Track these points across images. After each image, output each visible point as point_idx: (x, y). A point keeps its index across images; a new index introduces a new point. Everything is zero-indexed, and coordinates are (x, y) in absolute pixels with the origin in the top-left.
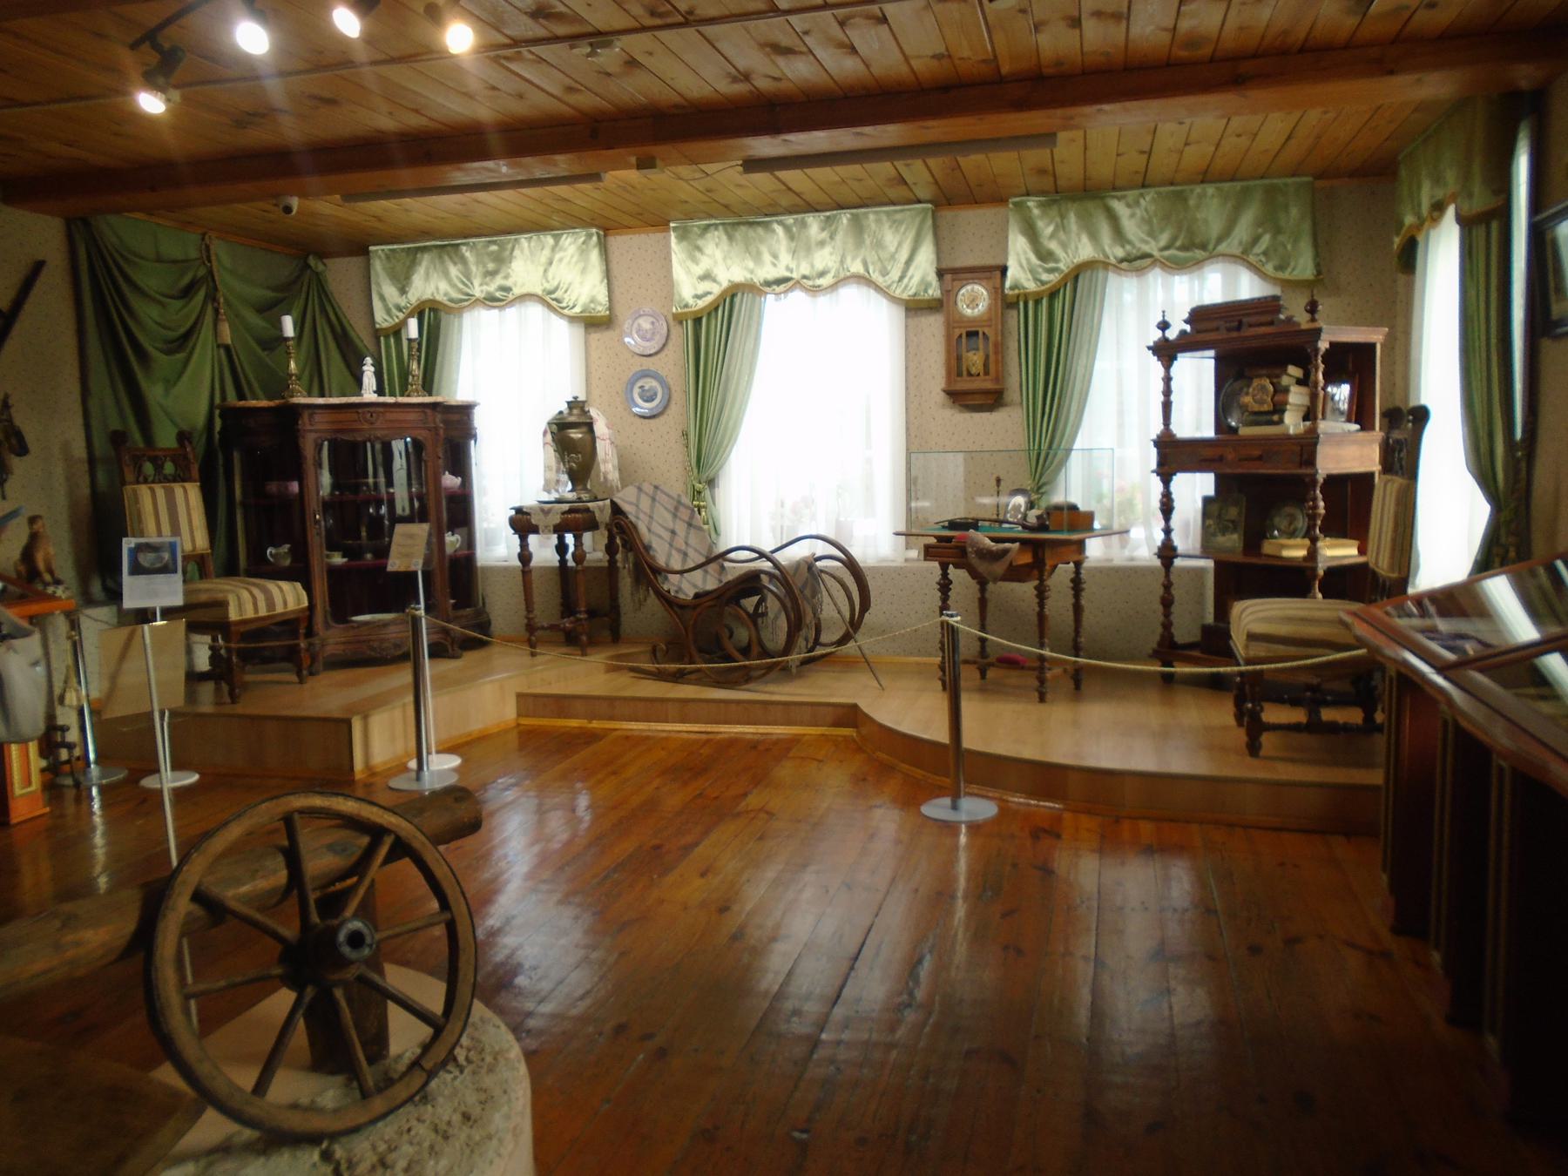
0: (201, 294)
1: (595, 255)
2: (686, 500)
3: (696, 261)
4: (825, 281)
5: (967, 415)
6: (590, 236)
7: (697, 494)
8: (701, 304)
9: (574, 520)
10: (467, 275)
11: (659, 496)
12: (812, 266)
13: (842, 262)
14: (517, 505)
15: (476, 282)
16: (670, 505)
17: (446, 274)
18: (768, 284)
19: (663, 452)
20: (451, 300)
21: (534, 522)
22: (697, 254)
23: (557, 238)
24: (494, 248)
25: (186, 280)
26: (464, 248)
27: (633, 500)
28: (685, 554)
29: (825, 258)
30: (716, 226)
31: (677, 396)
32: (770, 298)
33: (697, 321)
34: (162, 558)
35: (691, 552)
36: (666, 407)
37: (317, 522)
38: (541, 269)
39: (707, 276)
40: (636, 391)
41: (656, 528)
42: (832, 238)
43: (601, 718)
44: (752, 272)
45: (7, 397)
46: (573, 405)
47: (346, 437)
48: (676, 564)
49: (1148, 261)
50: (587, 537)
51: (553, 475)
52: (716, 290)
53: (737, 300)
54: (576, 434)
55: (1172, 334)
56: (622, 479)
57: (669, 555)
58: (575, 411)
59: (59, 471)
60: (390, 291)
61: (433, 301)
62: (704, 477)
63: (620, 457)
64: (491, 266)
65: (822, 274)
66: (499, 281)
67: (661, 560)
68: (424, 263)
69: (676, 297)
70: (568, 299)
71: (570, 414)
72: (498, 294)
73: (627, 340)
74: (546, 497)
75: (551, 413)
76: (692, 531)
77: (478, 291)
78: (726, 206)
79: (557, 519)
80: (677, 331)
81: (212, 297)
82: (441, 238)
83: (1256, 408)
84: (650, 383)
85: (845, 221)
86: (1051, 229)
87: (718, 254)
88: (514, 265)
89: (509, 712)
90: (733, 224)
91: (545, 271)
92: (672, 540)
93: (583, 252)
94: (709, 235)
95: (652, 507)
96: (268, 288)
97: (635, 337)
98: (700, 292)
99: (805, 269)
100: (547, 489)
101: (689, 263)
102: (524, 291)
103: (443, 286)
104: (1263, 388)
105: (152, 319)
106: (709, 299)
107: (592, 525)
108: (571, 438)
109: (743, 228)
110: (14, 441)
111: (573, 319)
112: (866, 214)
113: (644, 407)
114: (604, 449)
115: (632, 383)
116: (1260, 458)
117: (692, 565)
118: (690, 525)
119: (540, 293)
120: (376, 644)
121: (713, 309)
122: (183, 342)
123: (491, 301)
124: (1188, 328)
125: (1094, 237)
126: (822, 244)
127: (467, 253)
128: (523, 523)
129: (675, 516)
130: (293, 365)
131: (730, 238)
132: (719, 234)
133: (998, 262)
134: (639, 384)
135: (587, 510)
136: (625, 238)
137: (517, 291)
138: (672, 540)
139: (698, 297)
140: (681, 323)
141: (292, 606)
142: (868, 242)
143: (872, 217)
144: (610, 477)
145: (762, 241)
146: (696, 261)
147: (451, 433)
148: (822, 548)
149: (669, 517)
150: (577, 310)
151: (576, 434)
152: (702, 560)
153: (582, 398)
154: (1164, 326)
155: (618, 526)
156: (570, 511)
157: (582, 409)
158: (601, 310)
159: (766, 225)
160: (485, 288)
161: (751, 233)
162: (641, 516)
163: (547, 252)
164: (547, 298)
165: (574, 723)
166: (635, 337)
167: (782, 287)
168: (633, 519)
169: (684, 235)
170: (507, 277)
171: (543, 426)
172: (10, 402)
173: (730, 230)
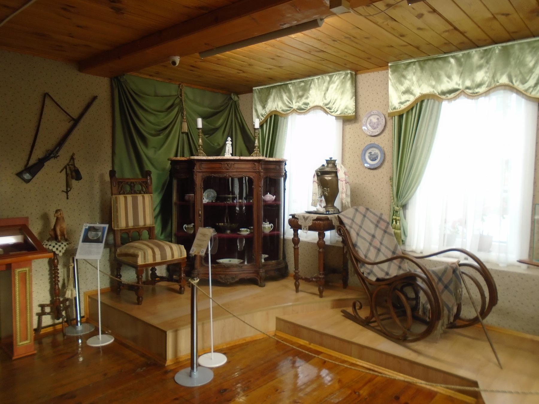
0: (176, 110)
1: (348, 84)
2: (386, 217)
3: (401, 83)
6: (347, 74)
7: (395, 212)
8: (403, 107)
10: (290, 98)
11: (369, 214)
12: (473, 81)
13: (493, 77)
14: (293, 213)
15: (294, 102)
16: (375, 219)
17: (281, 98)
18: (443, 93)
19: (379, 188)
20: (283, 111)
21: (299, 223)
22: (403, 79)
23: (331, 77)
24: (303, 84)
25: (169, 104)
26: (290, 85)
28: (379, 250)
29: (480, 76)
30: (414, 62)
31: (388, 158)
32: (445, 104)
33: (401, 117)
34: (97, 235)
35: (383, 249)
37: (199, 215)
38: (323, 93)
39: (408, 91)
41: (362, 233)
43: (315, 343)
44: (434, 87)
45: (73, 154)
47: (216, 175)
48: (372, 256)
50: (328, 234)
51: (318, 197)
52: (412, 99)
53: (424, 104)
54: (328, 178)
56: (352, 201)
57: (368, 250)
58: (330, 165)
59: (97, 187)
60: (259, 108)
61: (276, 111)
62: (400, 204)
63: (352, 191)
64: (300, 93)
65: (479, 85)
66: (304, 100)
67: (362, 255)
68: (273, 94)
69: (390, 104)
70: (335, 107)
71: (327, 166)
72: (303, 107)
73: (364, 128)
75: (318, 166)
76: (386, 235)
77: (295, 106)
78: (418, 48)
79: (310, 223)
81: (181, 110)
82: (280, 81)
84: (375, 151)
85: (497, 51)
87: (414, 78)
88: (311, 92)
89: (271, 327)
90: (424, 61)
91: (325, 94)
92: (372, 241)
93: (343, 83)
94: (410, 68)
95: (363, 221)
96: (210, 108)
97: (368, 125)
98: (403, 100)
99: (468, 83)
100: (314, 204)
101: (397, 85)
102: (315, 104)
103: (280, 104)
105: (149, 122)
106: (408, 104)
107: (331, 227)
109: (430, 62)
110: (74, 174)
111: (337, 117)
112: (512, 46)
113: (370, 162)
114: (342, 186)
117: (383, 258)
118: (385, 232)
119: (321, 104)
120: (223, 276)
121: (410, 109)
122: (165, 130)
123: (301, 111)
126: (480, 67)
127: (291, 87)
128: (295, 223)
129: (377, 226)
130: (200, 141)
131: (422, 68)
132: (417, 67)
134: (369, 151)
135: (327, 219)
136: (367, 74)
137: (311, 105)
138: (372, 241)
139: (402, 103)
141: (177, 256)
142: (513, 63)
143: (517, 47)
145: (441, 68)
146: (401, 83)
147: (273, 176)
148: (463, 259)
149: (372, 226)
150: (338, 113)
151: (328, 178)
152: (390, 255)
156: (318, 219)
158: (351, 112)
159: (445, 59)
160: (298, 104)
161: (435, 64)
162: (354, 226)
163: (326, 84)
164: (325, 108)
165: (302, 342)
166: (368, 125)
167: (452, 95)
168: (348, 227)
169: (395, 69)
170: (307, 98)
171: (314, 172)
172: (75, 157)
173: (422, 64)
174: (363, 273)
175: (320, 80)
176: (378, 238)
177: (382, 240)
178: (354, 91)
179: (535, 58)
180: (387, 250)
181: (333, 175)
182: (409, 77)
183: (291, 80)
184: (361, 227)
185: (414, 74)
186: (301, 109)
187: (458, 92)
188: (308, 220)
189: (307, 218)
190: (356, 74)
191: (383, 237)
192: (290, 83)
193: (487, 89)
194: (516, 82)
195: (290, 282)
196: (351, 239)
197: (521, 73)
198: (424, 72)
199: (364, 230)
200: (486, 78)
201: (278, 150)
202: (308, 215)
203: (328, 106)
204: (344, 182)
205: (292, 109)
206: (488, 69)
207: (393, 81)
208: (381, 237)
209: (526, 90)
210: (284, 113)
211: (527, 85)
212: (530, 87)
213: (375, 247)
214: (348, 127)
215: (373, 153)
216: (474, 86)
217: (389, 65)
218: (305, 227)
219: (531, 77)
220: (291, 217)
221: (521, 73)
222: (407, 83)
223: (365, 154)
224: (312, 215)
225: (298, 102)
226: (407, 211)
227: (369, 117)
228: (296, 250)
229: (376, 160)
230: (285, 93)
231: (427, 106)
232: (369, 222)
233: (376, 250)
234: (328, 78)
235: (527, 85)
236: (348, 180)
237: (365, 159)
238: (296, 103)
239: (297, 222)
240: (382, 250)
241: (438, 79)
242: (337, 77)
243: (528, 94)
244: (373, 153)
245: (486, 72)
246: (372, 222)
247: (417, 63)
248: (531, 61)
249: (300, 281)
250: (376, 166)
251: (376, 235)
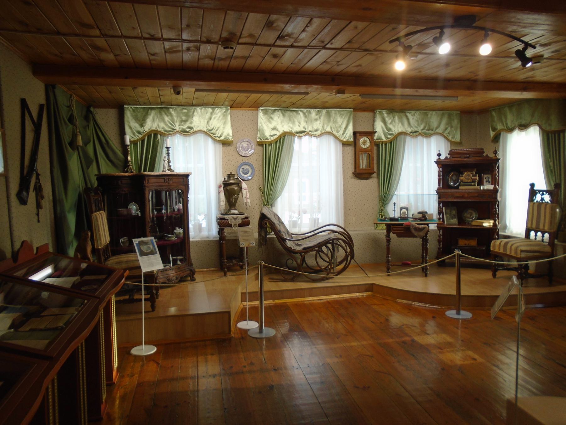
5: (359, 181)
38: (206, 121)
40: (241, 170)
49: (417, 133)
55: (442, 157)
83: (466, 181)
86: (390, 121)
94: (275, 113)
101: (268, 123)
104: (469, 175)
109: (289, 112)
115: (240, 167)
116: (477, 196)
124: (449, 156)
125: (403, 124)
131: (284, 115)
133: (370, 130)
134: (242, 167)
154: (439, 155)
189: (236, 218)
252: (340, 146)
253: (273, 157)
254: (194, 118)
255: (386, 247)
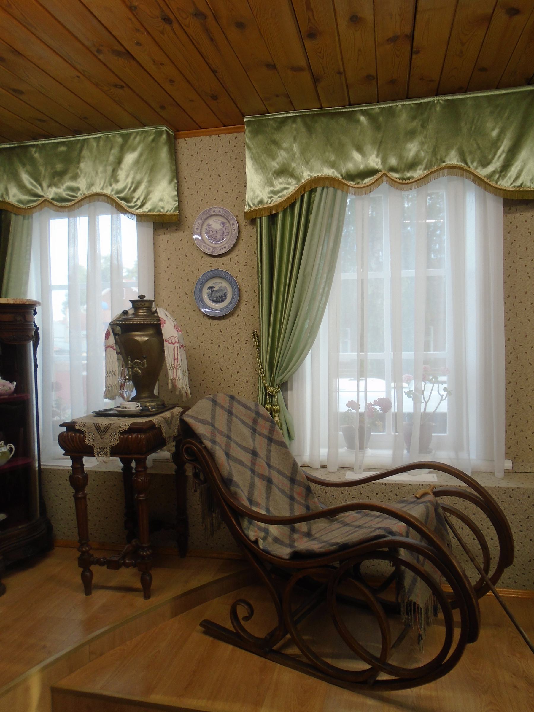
1: (164, 154)
4: (418, 173)
6: (160, 133)
7: (269, 397)
8: (277, 200)
9: (134, 444)
11: (237, 409)
13: (435, 152)
15: (45, 185)
18: (350, 177)
19: (234, 356)
20: (20, 201)
23: (125, 137)
24: (63, 149)
27: (207, 417)
29: (412, 149)
31: (248, 296)
33: (272, 218)
36: (236, 308)
38: (110, 169)
39: (284, 171)
40: (205, 292)
42: (423, 126)
46: (139, 304)
51: (118, 379)
52: (293, 187)
54: (141, 337)
56: (192, 386)
58: (141, 312)
63: (189, 357)
65: (412, 165)
71: (136, 314)
72: (64, 194)
74: (106, 404)
79: (115, 440)
80: (250, 234)
82: (11, 141)
87: (296, 148)
90: (313, 116)
92: (254, 463)
93: (152, 150)
94: (286, 128)
95: (229, 423)
97: (208, 233)
99: (393, 161)
100: (109, 394)
101: (264, 157)
108: (135, 339)
109: (324, 120)
111: (141, 219)
114: (174, 355)
115: (202, 283)
118: (270, 440)
121: (289, 205)
126: (411, 134)
128: (73, 440)
129: (254, 431)
131: (310, 130)
134: (210, 284)
135: (152, 426)
140: (253, 222)
142: (465, 130)
144: (179, 385)
149: (247, 432)
151: (141, 337)
153: (149, 297)
155: (190, 451)
156: (133, 429)
157: (149, 309)
159: (350, 116)
162: (219, 438)
163: (115, 151)
166: (208, 233)
167: (367, 181)
168: (208, 444)
169: (258, 129)
173: (309, 122)
174: (256, 542)
175: (101, 143)
176: (262, 456)
177: (268, 458)
178: (174, 167)
179: (500, 124)
180: (281, 477)
181: (151, 332)
182: (285, 145)
183: (35, 139)
184: (229, 437)
185: (295, 139)
186: (63, 200)
187: (376, 177)
188: (108, 435)
189: (107, 428)
190: (175, 138)
191: (269, 451)
192: (33, 146)
193: (426, 172)
194: (472, 162)
195: (61, 566)
196: (218, 469)
197: (479, 148)
198: (314, 136)
199: (237, 443)
200: (422, 154)
201: (12, 284)
202: (103, 421)
203: (122, 195)
204: (177, 345)
205: (41, 200)
206: (425, 137)
207: (254, 151)
208: (265, 452)
209: (490, 176)
210: (24, 206)
211: (490, 169)
212: (494, 172)
213: (262, 477)
214: (164, 238)
215: (216, 288)
216: (403, 166)
217: (245, 120)
218: (102, 449)
219: (495, 154)
220: (64, 429)
221: (479, 148)
222: (282, 155)
223: (201, 291)
224: (115, 420)
225: (56, 185)
226: (289, 392)
227: (206, 219)
228: (80, 501)
229: (223, 301)
230: (24, 165)
231: (322, 199)
232: (240, 425)
233: (265, 483)
234: (120, 140)
235: (490, 169)
236: (183, 342)
237: (202, 300)
238: (50, 186)
239: (82, 440)
240: (275, 481)
241: (341, 152)
242: (138, 139)
243: (493, 184)
244: (216, 288)
245: (422, 144)
246: (244, 423)
247: (299, 120)
248: (493, 129)
249: (94, 568)
250: (225, 313)
251: (258, 451)
252: (495, 207)
253: (285, 248)
254: (82, 165)
255: (119, 594)
